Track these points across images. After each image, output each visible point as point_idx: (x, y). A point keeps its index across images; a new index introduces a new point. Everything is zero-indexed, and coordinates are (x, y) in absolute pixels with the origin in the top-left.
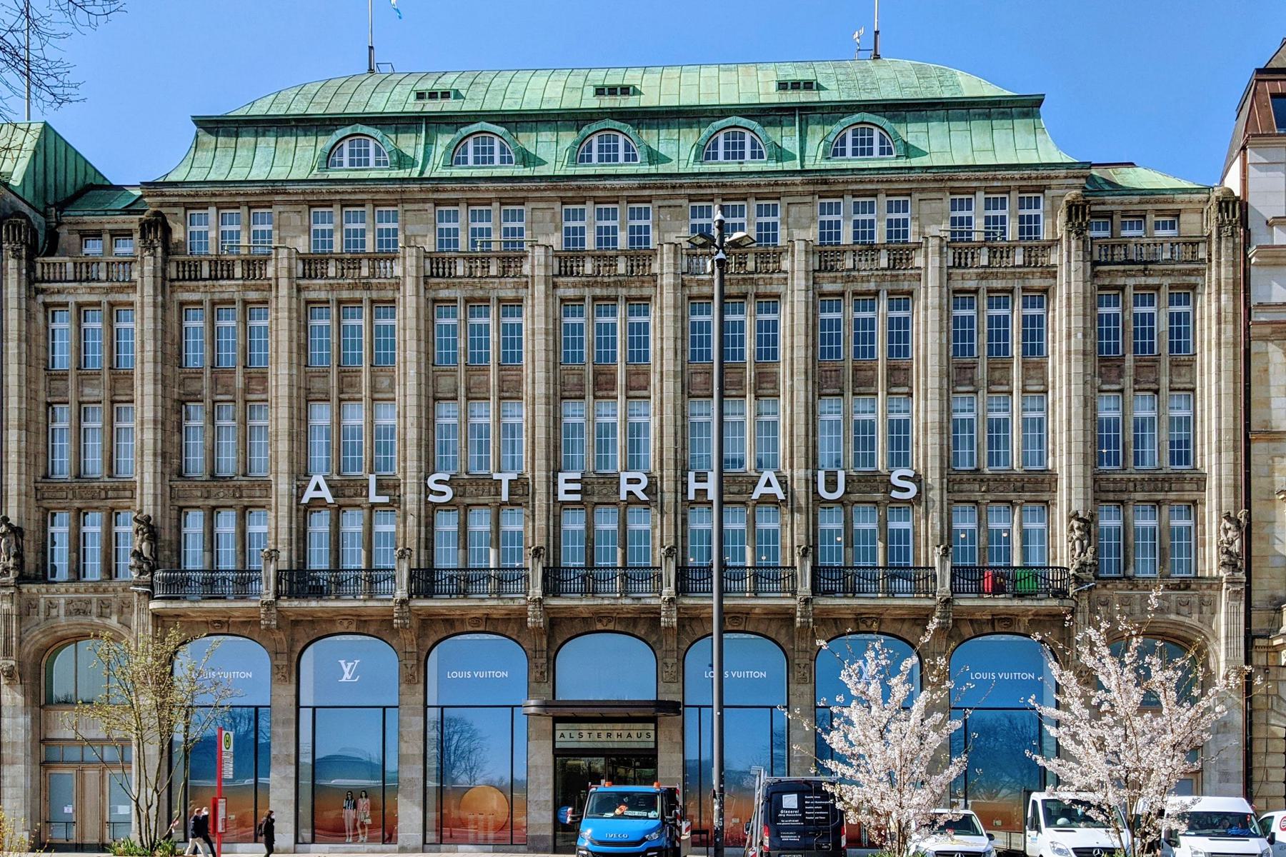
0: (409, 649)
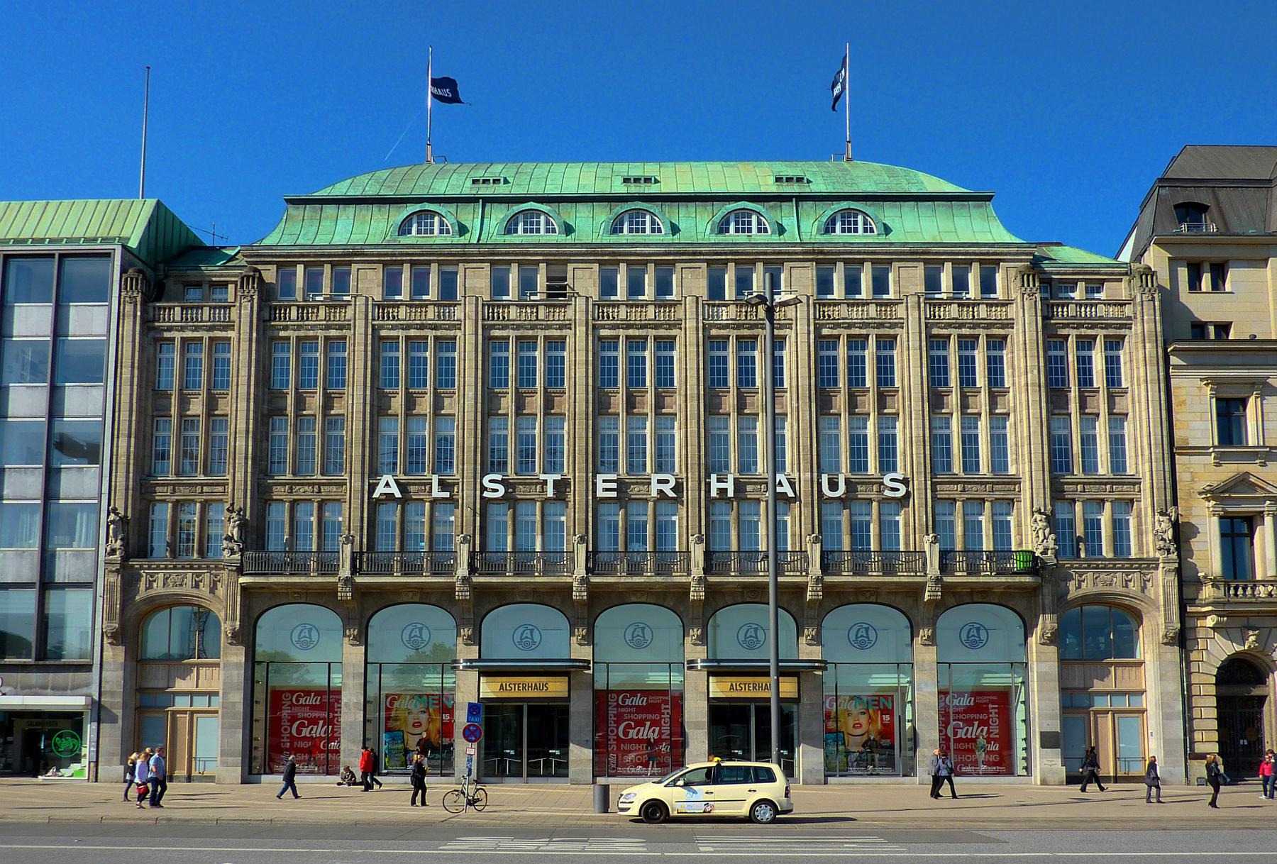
0: (466, 616)
